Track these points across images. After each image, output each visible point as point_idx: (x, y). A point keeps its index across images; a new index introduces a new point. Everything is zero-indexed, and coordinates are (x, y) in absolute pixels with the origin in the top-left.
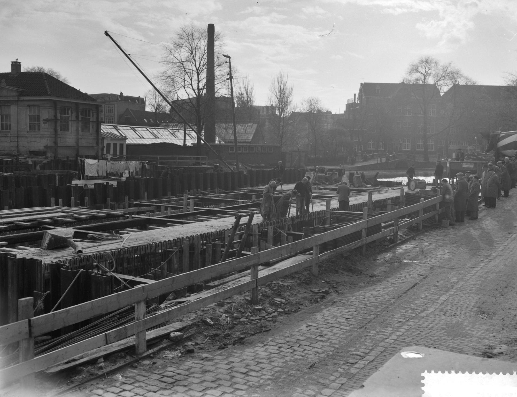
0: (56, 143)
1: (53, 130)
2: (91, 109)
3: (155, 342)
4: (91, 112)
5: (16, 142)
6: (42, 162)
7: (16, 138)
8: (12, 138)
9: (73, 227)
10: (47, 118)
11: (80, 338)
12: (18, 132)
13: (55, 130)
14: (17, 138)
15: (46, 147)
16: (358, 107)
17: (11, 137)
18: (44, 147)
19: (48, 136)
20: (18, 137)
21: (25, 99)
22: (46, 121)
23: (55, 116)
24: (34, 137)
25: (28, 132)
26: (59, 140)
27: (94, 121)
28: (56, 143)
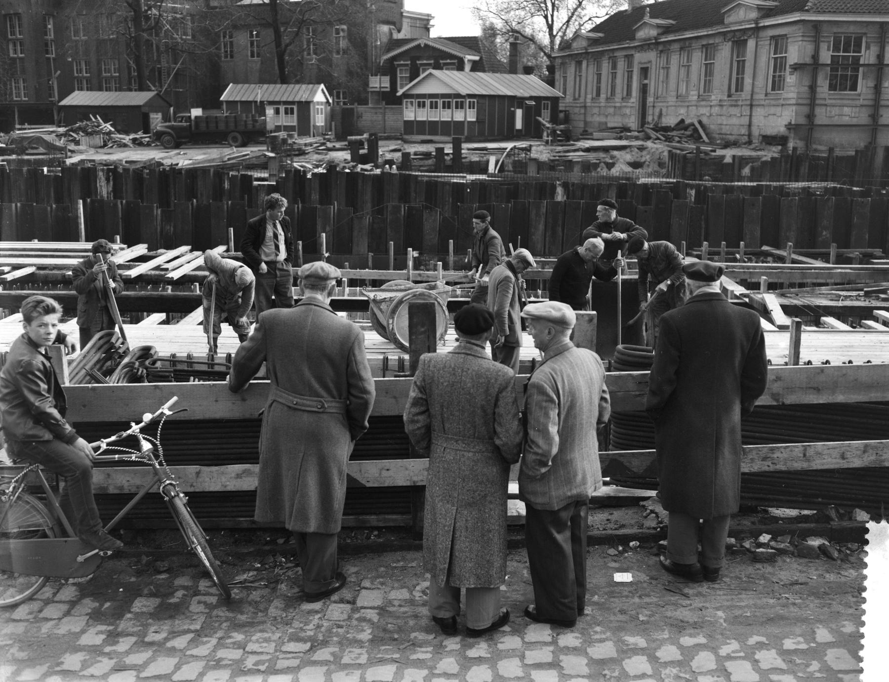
0: (810, 116)
1: (806, 88)
2: (865, 34)
3: (246, 551)
4: (864, 40)
5: (748, 117)
6: (760, 159)
7: (749, 107)
8: (743, 107)
9: (468, 340)
10: (796, 61)
11: (636, 433)
12: (752, 95)
13: (813, 88)
14: (751, 109)
15: (789, 126)
16: (619, 577)
17: (742, 106)
18: (786, 125)
19: (794, 102)
20: (751, 106)
21: (766, 24)
22: (796, 68)
23: (815, 57)
24: (774, 105)
25: (766, 95)
26: (818, 111)
27: (871, 62)
28: (810, 116)
